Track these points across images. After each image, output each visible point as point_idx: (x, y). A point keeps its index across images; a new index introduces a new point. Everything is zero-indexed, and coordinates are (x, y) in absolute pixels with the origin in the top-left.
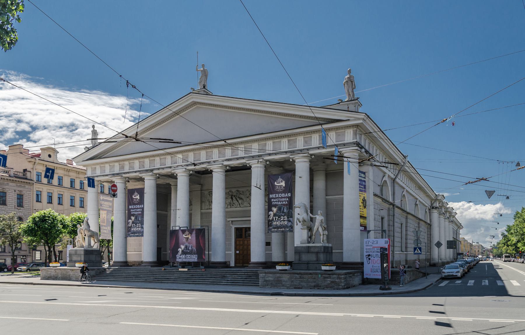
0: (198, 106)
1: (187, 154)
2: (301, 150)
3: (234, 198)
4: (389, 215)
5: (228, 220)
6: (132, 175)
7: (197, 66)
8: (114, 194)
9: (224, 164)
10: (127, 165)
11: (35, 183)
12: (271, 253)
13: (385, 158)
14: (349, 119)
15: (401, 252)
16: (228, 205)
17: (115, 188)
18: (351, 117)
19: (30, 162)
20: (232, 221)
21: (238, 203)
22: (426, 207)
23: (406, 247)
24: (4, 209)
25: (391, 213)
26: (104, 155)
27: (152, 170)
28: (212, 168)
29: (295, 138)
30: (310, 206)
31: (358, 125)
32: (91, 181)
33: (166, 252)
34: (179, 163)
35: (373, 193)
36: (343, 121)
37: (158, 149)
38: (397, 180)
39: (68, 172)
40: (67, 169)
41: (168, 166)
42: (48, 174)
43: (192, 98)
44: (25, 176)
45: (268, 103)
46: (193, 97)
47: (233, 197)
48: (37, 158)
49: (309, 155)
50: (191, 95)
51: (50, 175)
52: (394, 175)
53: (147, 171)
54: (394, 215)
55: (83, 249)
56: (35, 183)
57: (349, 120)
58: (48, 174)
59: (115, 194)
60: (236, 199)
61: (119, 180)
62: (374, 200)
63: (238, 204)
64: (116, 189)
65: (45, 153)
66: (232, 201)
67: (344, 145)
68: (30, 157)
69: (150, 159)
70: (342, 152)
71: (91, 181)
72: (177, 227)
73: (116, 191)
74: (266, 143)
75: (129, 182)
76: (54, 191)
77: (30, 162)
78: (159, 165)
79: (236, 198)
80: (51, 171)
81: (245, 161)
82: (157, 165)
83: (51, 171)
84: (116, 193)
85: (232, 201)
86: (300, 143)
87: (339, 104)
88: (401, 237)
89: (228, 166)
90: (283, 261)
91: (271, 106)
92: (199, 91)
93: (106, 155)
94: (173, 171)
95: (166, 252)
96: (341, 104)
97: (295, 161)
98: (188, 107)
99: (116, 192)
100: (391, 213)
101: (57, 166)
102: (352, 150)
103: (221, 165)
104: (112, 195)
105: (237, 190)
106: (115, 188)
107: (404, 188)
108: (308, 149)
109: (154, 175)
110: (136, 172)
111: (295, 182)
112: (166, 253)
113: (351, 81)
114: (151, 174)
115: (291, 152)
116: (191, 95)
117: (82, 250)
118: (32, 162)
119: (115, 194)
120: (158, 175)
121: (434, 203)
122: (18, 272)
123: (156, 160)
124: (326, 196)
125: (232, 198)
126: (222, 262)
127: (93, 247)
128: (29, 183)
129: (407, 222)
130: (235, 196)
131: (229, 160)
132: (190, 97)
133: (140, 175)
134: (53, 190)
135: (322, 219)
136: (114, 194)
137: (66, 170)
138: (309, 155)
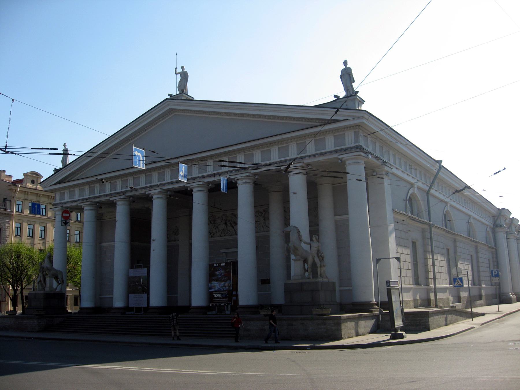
0: (176, 113)
3: (228, 224)
4: (424, 238)
5: (221, 252)
6: (102, 199)
7: (176, 68)
8: (66, 221)
10: (77, 194)
13: (410, 165)
14: (347, 118)
15: (491, 286)
16: (221, 233)
18: (349, 116)
20: (226, 253)
21: (234, 230)
22: (487, 225)
23: (479, 281)
25: (428, 235)
27: (124, 193)
29: (287, 145)
30: (310, 231)
31: (359, 126)
32: (36, 206)
33: (177, 294)
34: (154, 183)
36: (339, 121)
38: (432, 191)
39: (52, 200)
40: (52, 196)
43: (169, 105)
44: (4, 206)
45: (194, 102)
47: (227, 222)
50: (167, 102)
52: (427, 185)
53: (119, 194)
54: (431, 238)
55: (42, 292)
57: (347, 119)
60: (231, 225)
62: (394, 218)
63: (234, 232)
66: (227, 227)
67: (345, 150)
68: (12, 184)
69: (123, 179)
71: (36, 206)
72: (391, 259)
74: (253, 153)
75: (101, 207)
76: (24, 221)
79: (230, 223)
85: (227, 227)
87: (335, 102)
88: (490, 267)
89: (256, 174)
90: (164, 306)
91: (270, 109)
92: (177, 97)
93: (76, 177)
94: (147, 193)
95: (177, 294)
96: (337, 101)
100: (428, 235)
101: (41, 193)
102: (354, 156)
103: (201, 183)
104: (63, 222)
105: (232, 213)
107: (446, 203)
109: (127, 198)
110: (106, 196)
114: (123, 197)
116: (167, 102)
117: (42, 293)
120: (131, 199)
121: (497, 219)
122: (480, 306)
123: (129, 180)
124: (335, 216)
125: (226, 224)
129: (455, 247)
130: (229, 221)
131: (211, 176)
133: (111, 199)
134: (23, 220)
136: (66, 221)
137: (50, 197)
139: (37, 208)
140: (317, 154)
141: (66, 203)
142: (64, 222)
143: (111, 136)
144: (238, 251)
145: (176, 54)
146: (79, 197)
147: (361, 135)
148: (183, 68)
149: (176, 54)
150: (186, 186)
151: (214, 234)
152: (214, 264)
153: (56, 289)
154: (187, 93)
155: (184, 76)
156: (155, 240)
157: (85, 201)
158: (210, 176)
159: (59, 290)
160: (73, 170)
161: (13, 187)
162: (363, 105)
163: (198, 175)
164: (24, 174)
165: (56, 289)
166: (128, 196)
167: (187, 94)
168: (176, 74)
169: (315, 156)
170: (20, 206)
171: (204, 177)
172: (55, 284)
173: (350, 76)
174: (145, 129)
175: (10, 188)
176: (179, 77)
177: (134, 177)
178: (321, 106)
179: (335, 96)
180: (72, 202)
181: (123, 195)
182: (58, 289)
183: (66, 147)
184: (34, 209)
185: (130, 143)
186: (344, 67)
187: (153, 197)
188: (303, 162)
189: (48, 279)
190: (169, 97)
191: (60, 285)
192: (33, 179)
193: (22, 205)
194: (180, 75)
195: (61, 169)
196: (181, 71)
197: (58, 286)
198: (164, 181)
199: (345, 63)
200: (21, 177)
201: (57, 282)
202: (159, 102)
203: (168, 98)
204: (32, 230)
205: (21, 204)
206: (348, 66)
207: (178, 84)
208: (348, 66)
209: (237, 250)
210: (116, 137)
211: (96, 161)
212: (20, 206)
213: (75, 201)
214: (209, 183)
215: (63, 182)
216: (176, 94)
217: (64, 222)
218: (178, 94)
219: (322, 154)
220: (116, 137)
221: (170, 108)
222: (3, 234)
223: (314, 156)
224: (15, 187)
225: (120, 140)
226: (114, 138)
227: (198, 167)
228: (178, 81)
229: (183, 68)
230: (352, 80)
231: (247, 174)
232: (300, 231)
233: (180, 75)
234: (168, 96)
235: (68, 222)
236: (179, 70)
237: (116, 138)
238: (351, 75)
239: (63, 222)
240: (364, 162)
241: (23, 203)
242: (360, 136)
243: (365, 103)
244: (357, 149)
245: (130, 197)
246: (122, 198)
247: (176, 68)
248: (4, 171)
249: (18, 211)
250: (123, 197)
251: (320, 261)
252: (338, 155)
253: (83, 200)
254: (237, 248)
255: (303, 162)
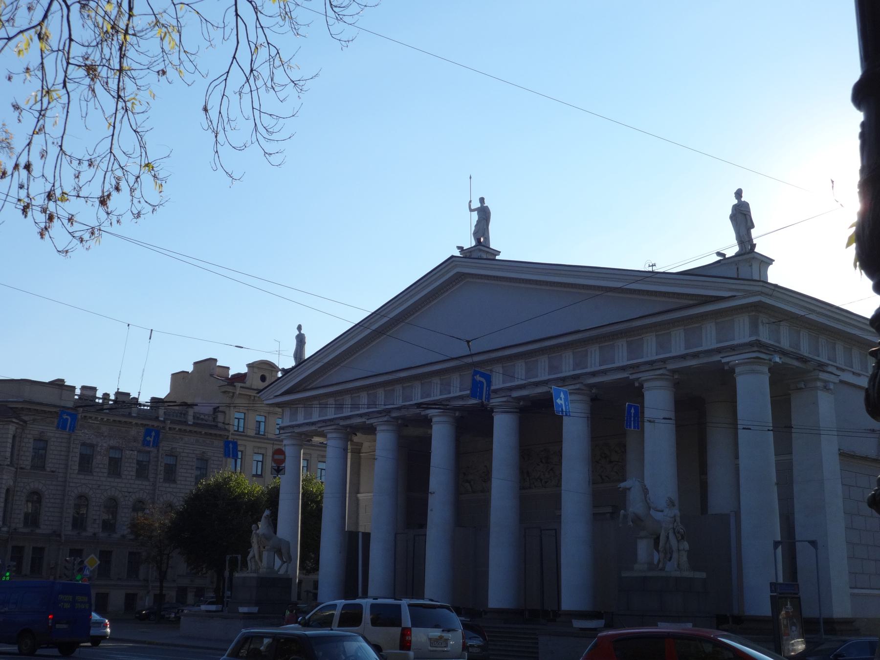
1: (583, 349)
2: (651, 363)
7: (470, 201)
8: (278, 467)
9: (668, 369)
11: (232, 434)
12: (771, 592)
17: (281, 457)
18: (737, 290)
19: (225, 392)
24: (170, 490)
26: (309, 385)
28: (431, 415)
32: (231, 445)
34: (434, 396)
35: (839, 450)
37: (448, 358)
41: (621, 364)
42: (148, 438)
46: (456, 265)
48: (239, 385)
49: (666, 373)
51: (152, 440)
53: (381, 413)
55: (255, 575)
56: (232, 434)
58: (148, 438)
59: (281, 468)
61: (384, 424)
64: (283, 458)
65: (256, 373)
67: (733, 348)
70: (325, 431)
71: (231, 445)
73: (283, 461)
77: (225, 392)
78: (401, 401)
80: (153, 434)
81: (627, 375)
82: (416, 398)
83: (153, 434)
84: (284, 465)
86: (650, 349)
93: (315, 383)
97: (376, 428)
98: (456, 279)
99: (283, 464)
102: (748, 359)
104: (275, 469)
106: (281, 457)
108: (664, 361)
111: (562, 441)
112: (772, 594)
113: (742, 213)
114: (385, 419)
115: (632, 367)
118: (229, 392)
119: (281, 468)
126: (576, 611)
127: (279, 571)
128: (220, 435)
132: (452, 264)
133: (368, 422)
135: (675, 516)
136: (278, 467)
138: (666, 373)
139: (232, 448)
140: (687, 355)
141: (299, 426)
142: (276, 468)
143: (356, 323)
144: (562, 514)
145: (470, 178)
146: (319, 416)
147: (762, 322)
148: (482, 200)
149: (470, 178)
150: (367, 423)
151: (546, 482)
152: (21, 653)
153: (279, 570)
154: (489, 245)
155: (484, 214)
156: (434, 493)
157: (328, 423)
158: (521, 388)
159: (283, 573)
160: (326, 360)
161: (230, 389)
162: (771, 266)
163: (502, 386)
164: (249, 366)
165: (279, 570)
166: (394, 418)
167: (488, 246)
168: (471, 210)
169: (685, 359)
170: (242, 421)
171: (511, 389)
172: (278, 562)
173: (746, 218)
174: (388, 327)
175: (224, 389)
176: (475, 216)
177: (405, 385)
178: (689, 272)
179: (719, 254)
180: (308, 424)
181: (385, 416)
182: (282, 572)
183: (302, 332)
184: (227, 449)
185: (342, 365)
186: (736, 202)
187: (433, 420)
188: (666, 368)
189: (265, 554)
190: (457, 253)
191: (286, 564)
192: (265, 374)
193: (244, 419)
194: (476, 212)
195: (293, 368)
196: (479, 205)
197: (282, 565)
198: (450, 393)
199: (739, 194)
200: (244, 370)
201: (281, 558)
202: (424, 275)
203: (455, 255)
204: (261, 463)
205: (243, 417)
206: (743, 199)
207: (473, 229)
208: (743, 199)
209: (561, 512)
210: (315, 360)
211: (327, 370)
212: (242, 421)
213: (313, 424)
214: (519, 399)
215: (295, 391)
216: (470, 247)
217: (276, 468)
218: (473, 247)
219: (695, 355)
220: (315, 360)
221: (458, 272)
222: (212, 470)
223: (683, 357)
224: (232, 387)
225: (323, 364)
226: (312, 362)
227: (501, 372)
228: (474, 223)
229: (482, 200)
230: (749, 224)
231: (578, 386)
232: (648, 488)
233: (476, 212)
234: (457, 249)
235: (282, 470)
236: (476, 204)
237: (317, 361)
238: (748, 217)
239: (275, 469)
240: (769, 369)
241: (247, 416)
242: (760, 324)
243: (773, 262)
244: (753, 346)
245: (396, 418)
246: (385, 421)
247: (470, 201)
248: (215, 360)
249: (237, 429)
250: (385, 419)
251: (678, 541)
252: (721, 357)
253: (324, 421)
254: (561, 509)
255: (666, 368)
